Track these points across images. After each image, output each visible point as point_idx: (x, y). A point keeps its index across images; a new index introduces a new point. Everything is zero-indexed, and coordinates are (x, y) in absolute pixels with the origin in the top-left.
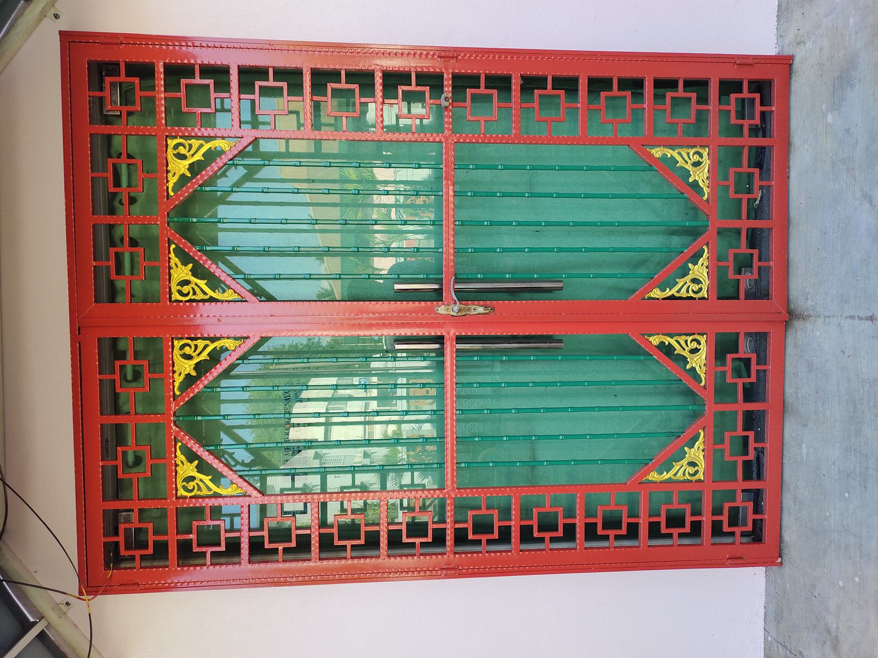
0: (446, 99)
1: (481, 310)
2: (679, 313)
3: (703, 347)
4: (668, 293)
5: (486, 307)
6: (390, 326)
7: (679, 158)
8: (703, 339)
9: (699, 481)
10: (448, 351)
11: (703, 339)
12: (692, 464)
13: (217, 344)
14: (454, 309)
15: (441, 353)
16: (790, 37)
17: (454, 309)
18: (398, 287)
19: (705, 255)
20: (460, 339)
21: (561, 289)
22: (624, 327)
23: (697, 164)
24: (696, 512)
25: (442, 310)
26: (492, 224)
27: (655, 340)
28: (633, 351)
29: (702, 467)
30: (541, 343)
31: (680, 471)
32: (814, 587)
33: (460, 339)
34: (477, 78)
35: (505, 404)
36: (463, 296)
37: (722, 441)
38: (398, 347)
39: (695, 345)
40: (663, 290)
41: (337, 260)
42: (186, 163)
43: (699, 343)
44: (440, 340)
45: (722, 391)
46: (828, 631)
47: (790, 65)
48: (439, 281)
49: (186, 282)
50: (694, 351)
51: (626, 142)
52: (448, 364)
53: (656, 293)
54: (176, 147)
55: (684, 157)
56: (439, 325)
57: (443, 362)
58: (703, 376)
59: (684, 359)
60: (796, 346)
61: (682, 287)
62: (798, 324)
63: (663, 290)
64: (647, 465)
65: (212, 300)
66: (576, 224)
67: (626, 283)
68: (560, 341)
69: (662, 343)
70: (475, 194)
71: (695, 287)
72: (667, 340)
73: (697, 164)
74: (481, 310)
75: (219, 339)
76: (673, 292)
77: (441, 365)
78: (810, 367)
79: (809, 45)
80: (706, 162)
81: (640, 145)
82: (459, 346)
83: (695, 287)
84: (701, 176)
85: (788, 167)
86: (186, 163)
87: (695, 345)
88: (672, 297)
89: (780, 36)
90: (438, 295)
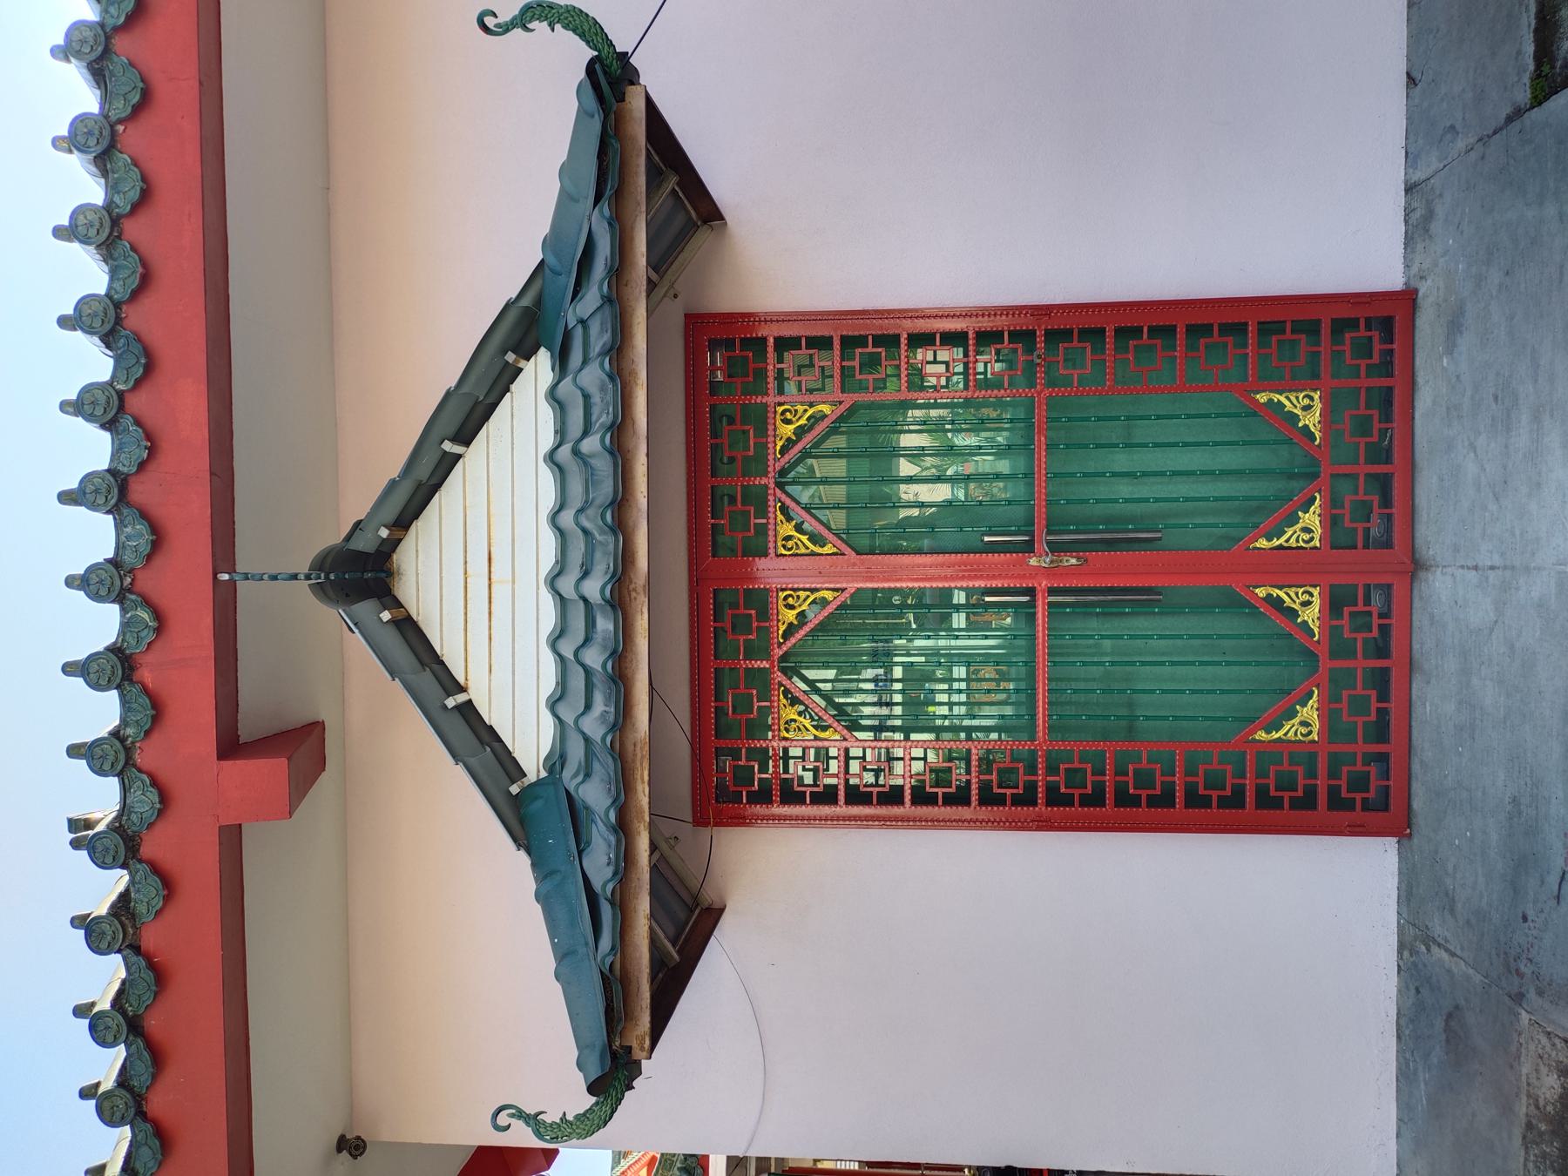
0: (1039, 357)
1: (1073, 561)
2: (1293, 567)
3: (1316, 600)
4: (1276, 542)
5: (1078, 559)
6: (981, 578)
7: (1287, 403)
8: (1316, 592)
9: (1313, 742)
10: (1040, 603)
11: (1316, 592)
12: (1304, 724)
13: (817, 595)
14: (1045, 562)
15: (1032, 604)
16: (1415, 269)
17: (1045, 562)
18: (986, 539)
19: (1317, 502)
20: (1052, 591)
21: (1159, 539)
22: (1224, 579)
23: (1306, 408)
24: (1312, 774)
25: (1033, 562)
26: (1085, 475)
27: (1261, 592)
28: (1239, 604)
29: (1316, 728)
30: (1142, 599)
31: (1290, 730)
32: (1436, 852)
33: (1052, 591)
34: (1071, 331)
35: (866, 487)
36: (1056, 548)
37: (1338, 701)
38: (987, 599)
39: (1307, 597)
40: (1269, 540)
41: (843, 462)
42: (792, 427)
43: (1311, 595)
44: (1031, 592)
45: (1339, 648)
46: (1447, 894)
47: (1414, 300)
48: (1031, 534)
49: (788, 538)
50: (1306, 604)
51: (1228, 388)
52: (1040, 615)
53: (1263, 543)
54: (785, 598)
55: (1291, 402)
56: (1031, 577)
57: (1034, 614)
58: (1316, 631)
59: (1295, 613)
60: (1421, 598)
61: (1291, 536)
62: (1422, 574)
63: (1269, 540)
64: (1253, 722)
65: (813, 554)
66: (1175, 473)
67: (1233, 532)
68: (1159, 594)
69: (1269, 595)
70: (1098, 446)
71: (1307, 537)
72: (1276, 592)
73: (1306, 408)
74: (1073, 561)
75: (817, 590)
76: (1282, 541)
77: (1032, 617)
78: (1432, 617)
79: (1429, 282)
80: (1318, 406)
81: (1247, 390)
82: (1051, 599)
83: (1307, 537)
84: (1312, 420)
85: (1413, 407)
86: (792, 427)
87: (1307, 597)
88: (1281, 547)
89: (1407, 267)
90: (1028, 548)
